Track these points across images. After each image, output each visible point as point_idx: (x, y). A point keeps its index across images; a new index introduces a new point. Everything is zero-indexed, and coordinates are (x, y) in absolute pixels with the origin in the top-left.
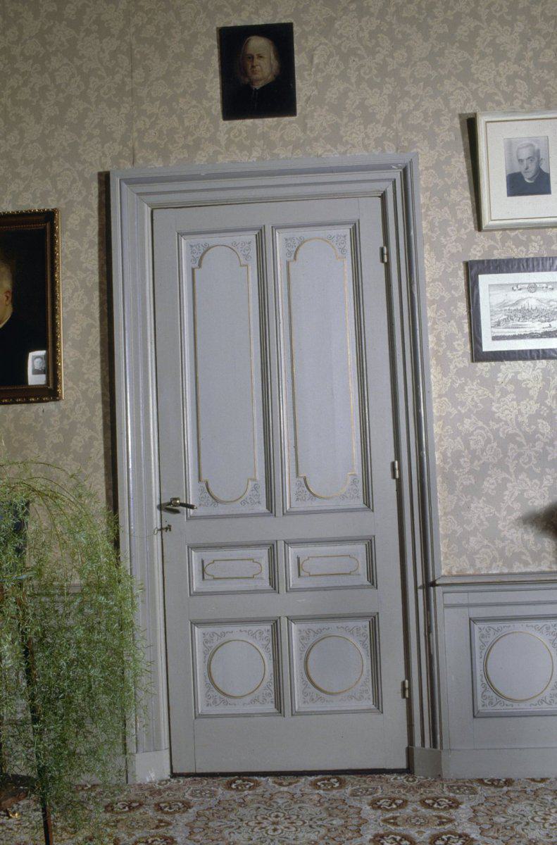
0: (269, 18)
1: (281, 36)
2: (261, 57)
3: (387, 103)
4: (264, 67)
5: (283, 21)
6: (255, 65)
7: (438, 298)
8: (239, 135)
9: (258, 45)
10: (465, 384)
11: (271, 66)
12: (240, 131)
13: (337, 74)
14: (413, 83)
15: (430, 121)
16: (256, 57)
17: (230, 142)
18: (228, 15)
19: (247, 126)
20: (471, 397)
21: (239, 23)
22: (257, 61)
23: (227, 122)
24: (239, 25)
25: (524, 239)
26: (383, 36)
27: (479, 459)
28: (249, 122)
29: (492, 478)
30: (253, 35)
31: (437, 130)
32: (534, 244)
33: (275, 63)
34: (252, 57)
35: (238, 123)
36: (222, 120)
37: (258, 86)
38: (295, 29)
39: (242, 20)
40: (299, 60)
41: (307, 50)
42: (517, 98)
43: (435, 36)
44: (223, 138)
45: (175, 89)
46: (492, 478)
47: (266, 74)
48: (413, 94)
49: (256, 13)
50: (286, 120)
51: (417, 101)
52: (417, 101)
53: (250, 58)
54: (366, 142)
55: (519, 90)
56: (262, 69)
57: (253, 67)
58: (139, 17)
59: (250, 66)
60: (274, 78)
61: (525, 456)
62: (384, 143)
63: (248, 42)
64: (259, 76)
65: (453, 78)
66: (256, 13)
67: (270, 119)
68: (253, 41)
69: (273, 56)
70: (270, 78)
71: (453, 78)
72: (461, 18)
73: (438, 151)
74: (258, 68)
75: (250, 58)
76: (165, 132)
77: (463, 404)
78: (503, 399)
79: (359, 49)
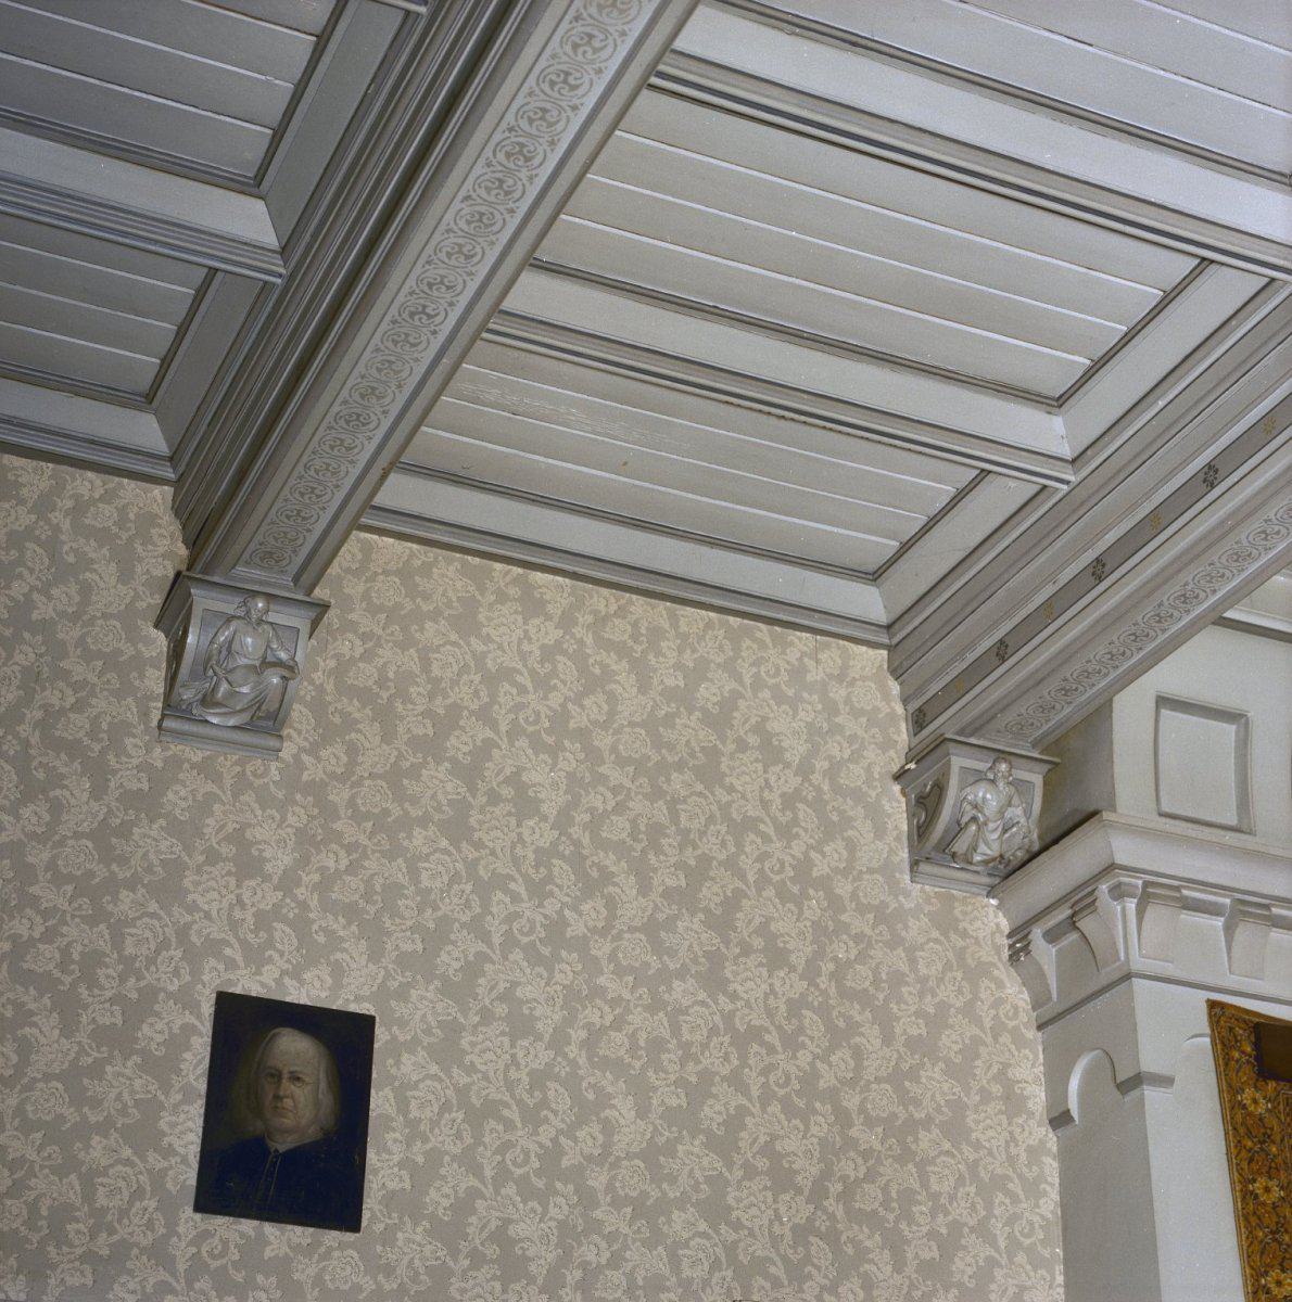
0: (324, 995)
1: (348, 1041)
2: (298, 1079)
3: (291, 844)
4: (300, 1104)
5: (353, 1008)
6: (281, 1093)
7: (79, 873)
8: (222, 1255)
9: (294, 1048)
10: (109, 1060)
11: (317, 1104)
12: (225, 1243)
13: (195, 759)
14: (349, 818)
15: (129, 529)
16: (286, 1076)
17: (197, 1267)
18: (231, 965)
19: (242, 1235)
20: (118, 1090)
21: (255, 990)
22: (288, 1087)
23: (198, 1216)
24: (254, 994)
25: (280, 795)
26: (558, 1087)
27: (111, 1231)
28: (248, 1226)
29: (133, 1277)
30: (292, 1026)
31: (140, 549)
32: (297, 809)
33: (327, 1100)
34: (277, 1076)
35: (220, 1222)
36: (189, 1210)
37: (282, 1144)
38: (378, 1031)
39: (263, 985)
40: (380, 1101)
41: (397, 1084)
42: (551, 894)
43: (407, 736)
44: (182, 1251)
45: (86, 1109)
46: (133, 1277)
47: (304, 1122)
48: (609, 1229)
49: (296, 974)
50: (332, 1237)
51: (355, 856)
52: (355, 856)
53: (272, 1075)
54: (238, 914)
55: (559, 881)
56: (295, 1107)
57: (277, 1098)
58: (24, 921)
59: (271, 1096)
60: (320, 1135)
61: (216, 1240)
62: (27, 544)
63: (274, 1035)
64: (288, 1122)
65: (432, 828)
66: (296, 974)
67: (299, 1229)
68: (285, 1039)
69: (323, 1085)
70: (312, 1134)
71: (432, 828)
72: (713, 1084)
73: (385, 968)
74: (288, 1103)
75: (272, 1075)
76: (44, 1212)
77: (96, 1103)
78: (186, 1108)
79: (507, 1105)
